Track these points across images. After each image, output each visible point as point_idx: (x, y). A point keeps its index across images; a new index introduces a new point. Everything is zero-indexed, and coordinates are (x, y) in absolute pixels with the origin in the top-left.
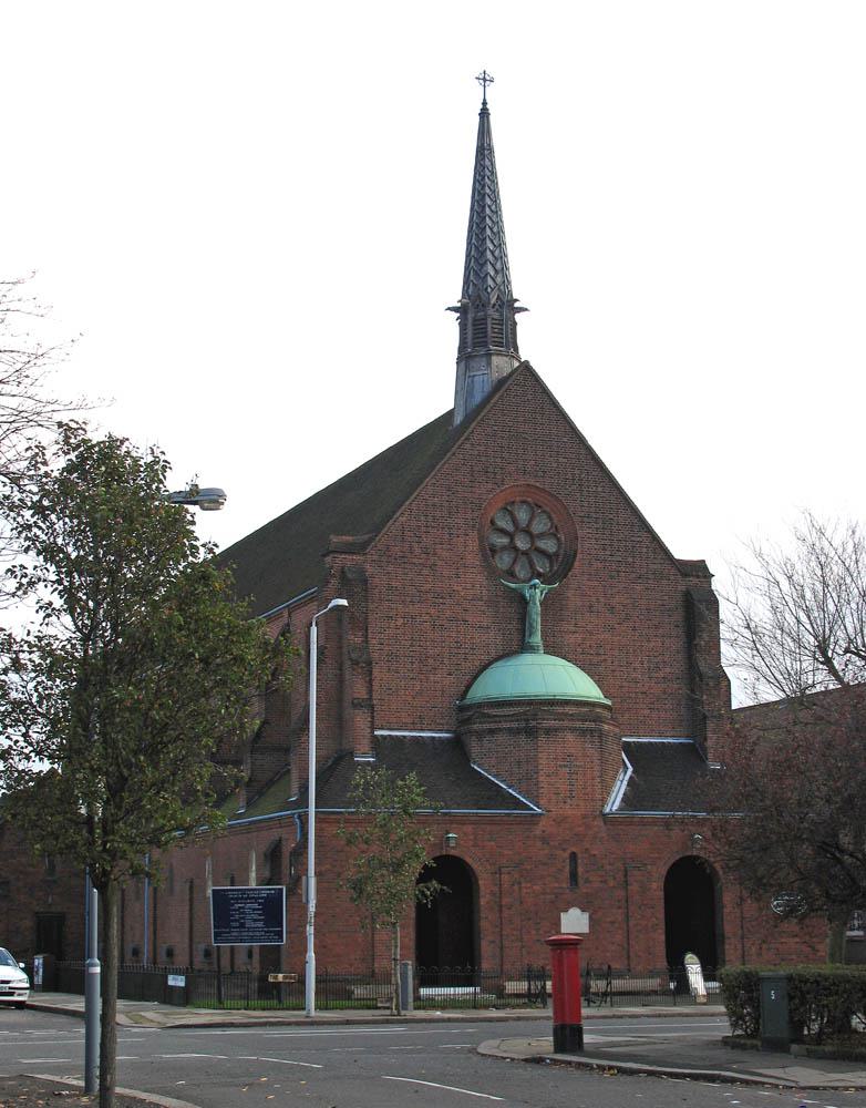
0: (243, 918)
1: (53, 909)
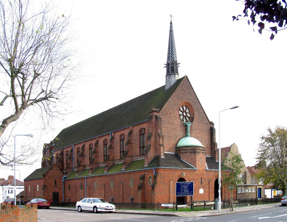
0: (184, 190)
1: (56, 191)
